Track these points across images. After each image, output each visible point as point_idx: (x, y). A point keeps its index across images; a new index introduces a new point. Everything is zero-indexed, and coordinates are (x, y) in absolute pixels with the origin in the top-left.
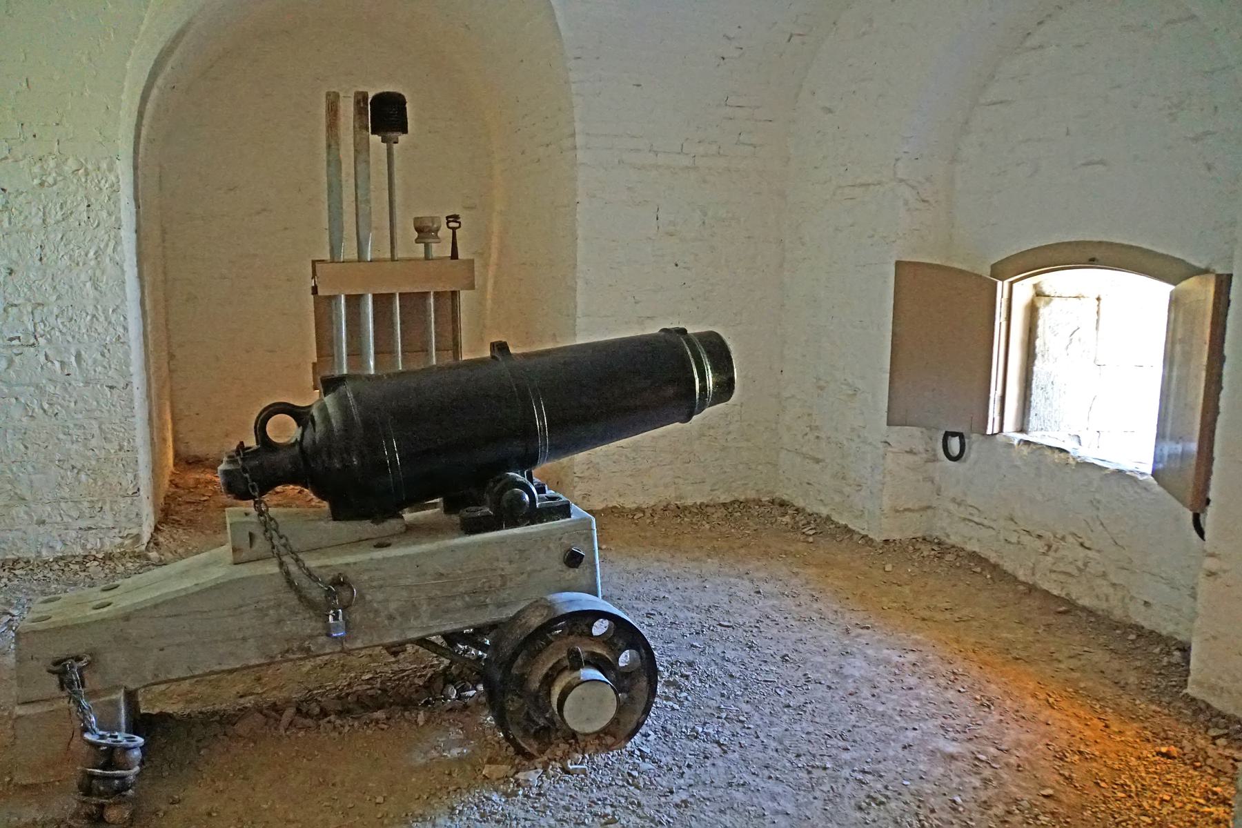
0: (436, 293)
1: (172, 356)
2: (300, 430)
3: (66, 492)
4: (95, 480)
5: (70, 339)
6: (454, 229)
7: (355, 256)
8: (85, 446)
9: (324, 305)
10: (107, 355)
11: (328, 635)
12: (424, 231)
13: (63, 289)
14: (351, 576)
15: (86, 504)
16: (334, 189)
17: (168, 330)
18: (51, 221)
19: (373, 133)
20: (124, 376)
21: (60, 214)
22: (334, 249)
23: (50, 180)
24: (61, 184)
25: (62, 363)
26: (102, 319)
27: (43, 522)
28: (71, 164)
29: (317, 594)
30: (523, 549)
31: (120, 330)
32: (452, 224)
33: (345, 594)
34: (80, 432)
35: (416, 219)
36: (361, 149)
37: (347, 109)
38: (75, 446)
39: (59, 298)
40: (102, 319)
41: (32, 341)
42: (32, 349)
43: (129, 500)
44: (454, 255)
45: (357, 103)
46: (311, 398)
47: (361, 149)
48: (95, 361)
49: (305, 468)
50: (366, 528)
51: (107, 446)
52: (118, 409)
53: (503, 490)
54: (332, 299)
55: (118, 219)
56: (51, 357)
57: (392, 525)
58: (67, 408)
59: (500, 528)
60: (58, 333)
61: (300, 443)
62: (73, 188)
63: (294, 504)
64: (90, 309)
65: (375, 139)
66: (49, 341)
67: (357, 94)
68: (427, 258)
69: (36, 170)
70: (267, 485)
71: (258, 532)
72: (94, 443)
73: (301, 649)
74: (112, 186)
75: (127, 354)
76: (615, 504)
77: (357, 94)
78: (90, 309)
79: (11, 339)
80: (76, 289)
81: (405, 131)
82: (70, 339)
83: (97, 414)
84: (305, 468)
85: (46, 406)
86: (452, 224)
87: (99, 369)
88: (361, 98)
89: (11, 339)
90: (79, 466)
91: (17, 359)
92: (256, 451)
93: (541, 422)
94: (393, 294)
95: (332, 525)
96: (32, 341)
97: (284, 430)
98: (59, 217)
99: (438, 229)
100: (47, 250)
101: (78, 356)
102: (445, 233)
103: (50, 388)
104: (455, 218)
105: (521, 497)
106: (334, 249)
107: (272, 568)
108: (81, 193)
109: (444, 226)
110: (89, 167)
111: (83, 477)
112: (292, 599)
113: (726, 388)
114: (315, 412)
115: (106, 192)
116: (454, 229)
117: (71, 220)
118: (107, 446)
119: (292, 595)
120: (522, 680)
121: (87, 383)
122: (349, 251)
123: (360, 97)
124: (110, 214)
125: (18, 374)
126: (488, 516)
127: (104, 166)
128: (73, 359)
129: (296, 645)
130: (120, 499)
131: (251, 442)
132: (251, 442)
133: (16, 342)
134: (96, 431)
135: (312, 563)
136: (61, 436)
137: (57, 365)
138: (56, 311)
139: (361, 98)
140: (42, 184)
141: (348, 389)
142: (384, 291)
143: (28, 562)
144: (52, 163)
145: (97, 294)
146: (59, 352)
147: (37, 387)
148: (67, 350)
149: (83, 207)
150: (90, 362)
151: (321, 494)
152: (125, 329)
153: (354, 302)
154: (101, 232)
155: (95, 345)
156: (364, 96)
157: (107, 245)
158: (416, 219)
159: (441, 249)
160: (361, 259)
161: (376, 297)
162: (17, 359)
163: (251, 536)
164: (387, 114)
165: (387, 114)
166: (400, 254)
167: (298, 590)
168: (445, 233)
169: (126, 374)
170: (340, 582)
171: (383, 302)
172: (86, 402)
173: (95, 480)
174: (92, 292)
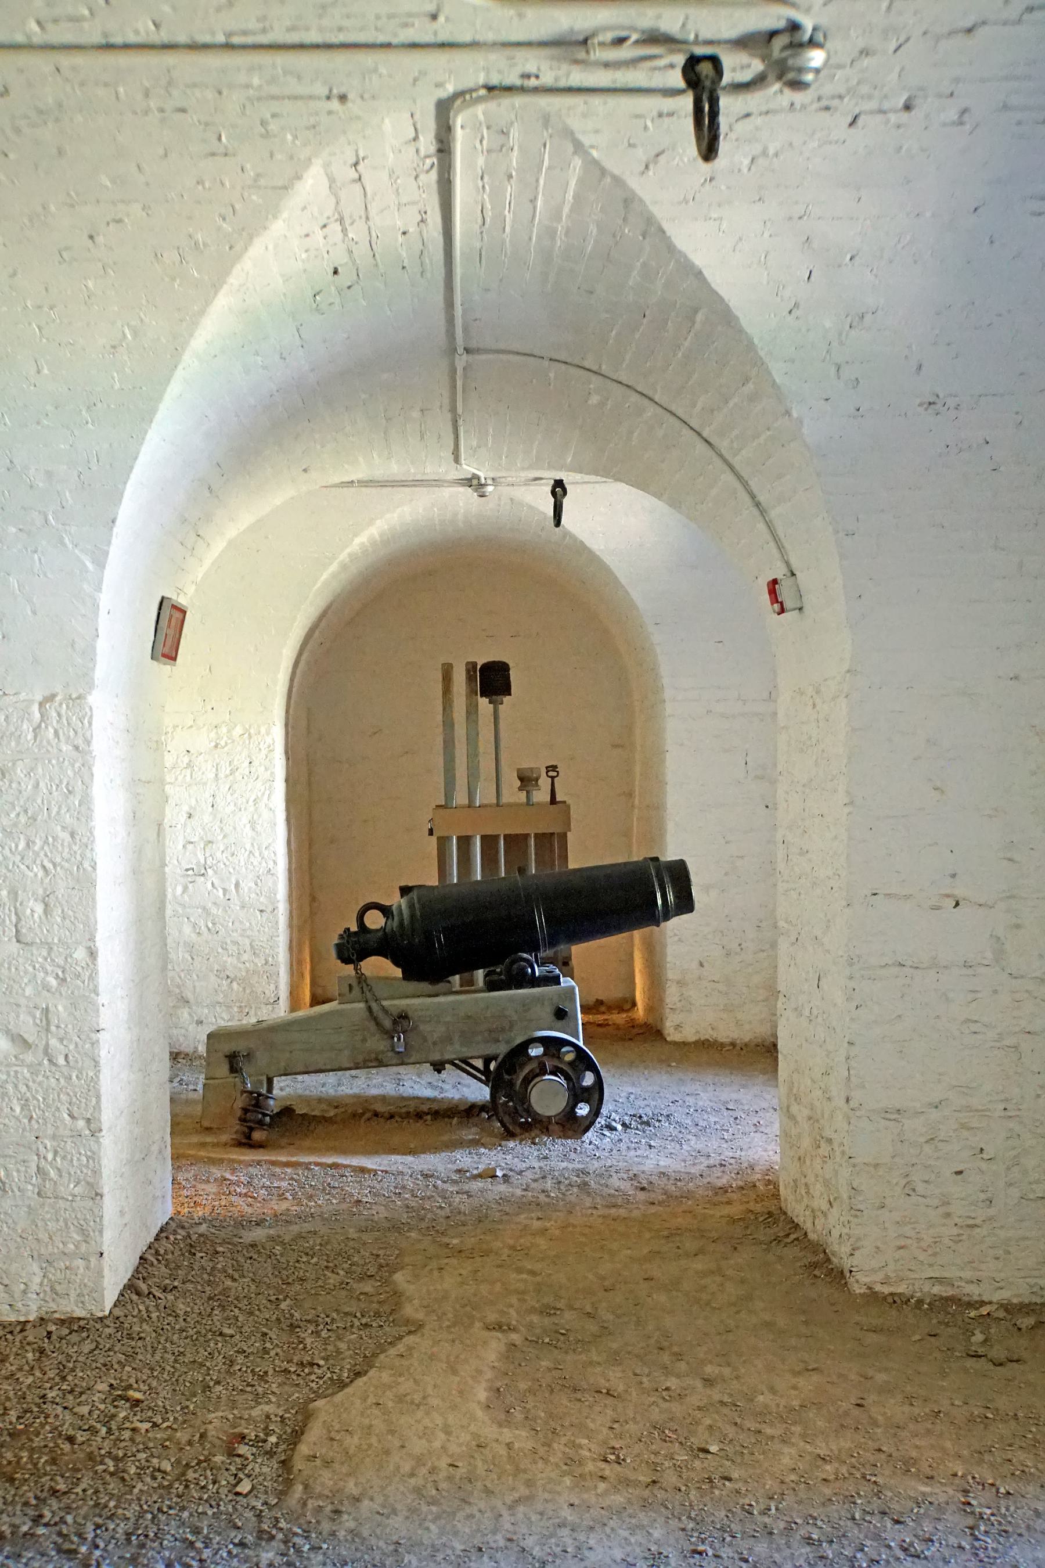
0: (536, 834)
1: (313, 899)
2: (384, 920)
3: (220, 998)
4: (244, 989)
5: (231, 870)
6: (553, 778)
7: (467, 802)
8: (238, 959)
9: (443, 843)
10: (259, 884)
11: (393, 1050)
12: (526, 780)
13: (228, 829)
14: (410, 1014)
15: (236, 1009)
16: (449, 744)
18: (221, 775)
19: (481, 696)
20: (273, 903)
21: (229, 769)
22: (449, 793)
23: (223, 743)
24: (229, 746)
25: (225, 890)
26: (257, 854)
27: (201, 1022)
28: (239, 730)
29: (387, 1023)
30: (526, 1005)
31: (271, 865)
32: (551, 774)
33: (405, 1023)
34: (235, 948)
35: (518, 770)
36: (472, 711)
37: (460, 677)
38: (229, 960)
39: (225, 837)
40: (257, 854)
41: (203, 871)
42: (202, 878)
43: (270, 1007)
44: (553, 800)
45: (468, 671)
46: (395, 900)
47: (472, 711)
48: (250, 888)
49: (385, 945)
50: (424, 986)
51: (256, 960)
52: (266, 930)
53: (513, 962)
54: (448, 839)
55: (272, 773)
56: (216, 884)
57: (441, 986)
58: (226, 927)
59: (511, 989)
60: (223, 866)
61: (383, 929)
62: (239, 748)
63: (379, 967)
64: (248, 847)
65: (483, 702)
66: (216, 872)
67: (468, 663)
68: (528, 803)
69: (213, 735)
70: (363, 954)
71: (355, 984)
72: (245, 957)
73: (377, 1059)
74: (269, 747)
75: (275, 883)
76: (707, 1037)
77: (468, 663)
78: (248, 847)
79: (187, 870)
80: (238, 829)
81: (510, 694)
82: (231, 870)
83: (249, 933)
84: (385, 945)
85: (210, 925)
86: (551, 774)
87: (253, 895)
88: (471, 667)
89: (187, 870)
90: (232, 976)
91: (190, 886)
92: (355, 933)
93: (540, 920)
94: (497, 837)
95: (405, 983)
96: (203, 871)
97: (375, 921)
98: (228, 772)
99: (537, 779)
100: (217, 798)
101: (237, 885)
102: (544, 782)
103: (214, 911)
104: (554, 768)
105: (524, 968)
106: (449, 793)
107: (362, 1005)
108: (245, 753)
109: (543, 774)
110: (252, 731)
111: (235, 985)
112: (372, 1026)
113: (685, 903)
114: (394, 908)
115: (264, 752)
116: (553, 778)
117: (237, 774)
118: (256, 960)
119: (373, 1023)
120: (511, 1084)
121: (243, 907)
122: (460, 798)
123: (470, 666)
124: (266, 769)
125: (190, 896)
126: (502, 980)
127: (263, 730)
128: (233, 887)
129: (373, 1056)
130: (263, 1006)
131: (354, 928)
132: (354, 928)
133: (190, 872)
134: (248, 948)
135: (385, 1003)
136: (220, 950)
137: (221, 892)
138: (222, 848)
139: (471, 667)
140: (216, 746)
141: (414, 895)
142: (489, 832)
143: (187, 1055)
144: (224, 729)
145: (254, 834)
146: (222, 880)
147: (204, 908)
148: (229, 879)
149: (247, 763)
150: (246, 890)
151: (396, 963)
152: (275, 863)
153: (465, 842)
154: (259, 783)
155: (250, 876)
156: (474, 664)
157: (263, 794)
158: (518, 770)
159: (541, 795)
160: (470, 806)
161: (484, 838)
162: (190, 886)
163: (350, 986)
164: (493, 680)
165: (493, 680)
166: (505, 799)
167: (375, 1019)
168: (544, 782)
169: (273, 902)
170: (403, 1017)
171: (490, 842)
172: (241, 922)
173: (244, 989)
174: (250, 833)
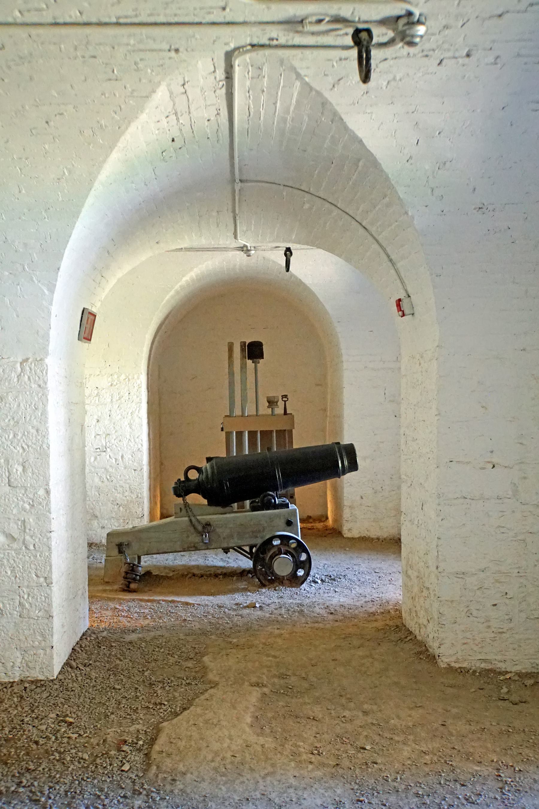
0: (276, 431)
2: (198, 475)
3: (114, 515)
4: (126, 510)
5: (119, 449)
6: (285, 401)
7: (241, 414)
8: (123, 495)
9: (228, 435)
10: (134, 456)
11: (203, 542)
12: (272, 403)
13: (117, 428)
14: (211, 523)
15: (122, 521)
16: (231, 384)
17: (146, 51)
18: (114, 400)
19: (248, 359)
20: (141, 466)
21: (118, 397)
22: (232, 409)
23: (115, 383)
24: (118, 385)
25: (116, 459)
26: (133, 441)
27: (104, 527)
28: (123, 377)
29: (200, 528)
30: (271, 518)
31: (140, 446)
32: (284, 399)
33: (209, 528)
34: (121, 489)
35: (267, 397)
36: (243, 367)
37: (237, 349)
38: (118, 495)
39: (116, 432)
40: (133, 441)
41: (105, 449)
42: (104, 453)
43: (139, 520)
44: (285, 413)
45: (241, 346)
46: (204, 464)
47: (243, 367)
48: (129, 458)
49: (199, 488)
50: (219, 509)
51: (132, 496)
52: (137, 480)
53: (265, 497)
54: (231, 433)
55: (140, 399)
56: (112, 456)
57: (228, 509)
58: (117, 478)
59: (263, 510)
60: (115, 447)
61: (198, 479)
62: (123, 386)
63: (196, 499)
64: (128, 437)
65: (249, 362)
66: (111, 450)
67: (241, 342)
68: (272, 415)
69: (110, 379)
70: (187, 492)
71: (183, 508)
72: (126, 494)
73: (194, 547)
74: (139, 385)
75: (142, 456)
76: (365, 535)
77: (241, 342)
78: (128, 437)
79: (96, 449)
80: (123, 428)
81: (263, 358)
82: (119, 449)
83: (128, 481)
84: (199, 488)
85: (108, 477)
86: (284, 399)
87: (130, 462)
88: (243, 344)
89: (96, 449)
90: (120, 503)
91: (98, 457)
92: (183, 481)
93: (278, 474)
94: (256, 432)
95: (209, 507)
96: (105, 449)
97: (193, 475)
98: (118, 398)
99: (277, 402)
100: (112, 412)
101: (122, 457)
102: (281, 404)
103: (110, 470)
104: (286, 396)
105: (270, 500)
106: (232, 409)
107: (187, 519)
108: (126, 389)
109: (280, 399)
110: (130, 377)
111: (121, 508)
112: (192, 529)
113: (353, 466)
114: (203, 469)
115: (136, 388)
116: (285, 401)
117: (122, 399)
118: (132, 496)
119: (192, 528)
120: (264, 559)
121: (125, 468)
122: (237, 412)
123: (243, 344)
124: (137, 397)
125: (98, 463)
126: (259, 506)
127: (136, 377)
128: (120, 458)
129: (192, 545)
130: (136, 519)
131: (183, 479)
132: (183, 479)
133: (98, 450)
134: (128, 489)
135: (198, 518)
136: (113, 490)
137: (114, 460)
138: (114, 438)
139: (243, 344)
140: (111, 385)
141: (214, 462)
142: (252, 429)
143: (97, 544)
144: (116, 376)
145: (131, 430)
146: (115, 454)
147: (105, 469)
148: (118, 453)
149: (127, 394)
150: (127, 459)
151: (204, 497)
152: (142, 445)
153: (240, 434)
154: (134, 404)
155: (129, 452)
156: (245, 343)
157: (136, 410)
158: (267, 397)
159: (279, 410)
160: (243, 416)
161: (249, 432)
162: (98, 457)
163: (181, 509)
164: (254, 351)
165: (254, 351)
166: (261, 412)
167: (194, 526)
168: (281, 404)
169: (141, 465)
170: (208, 524)
171: (253, 435)
172: (124, 476)
173: (126, 510)
174: (129, 430)
